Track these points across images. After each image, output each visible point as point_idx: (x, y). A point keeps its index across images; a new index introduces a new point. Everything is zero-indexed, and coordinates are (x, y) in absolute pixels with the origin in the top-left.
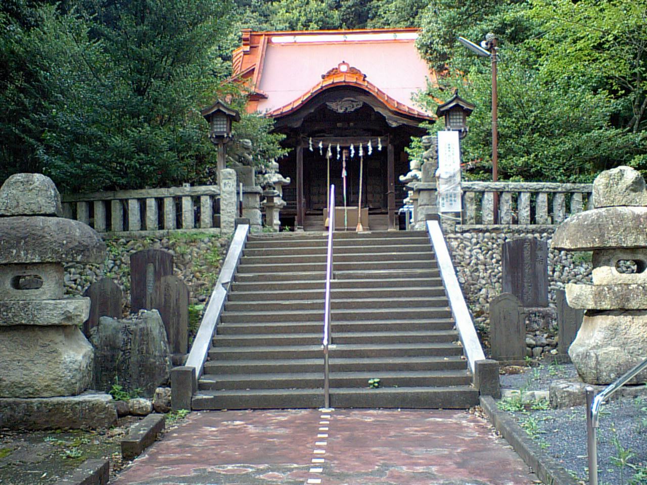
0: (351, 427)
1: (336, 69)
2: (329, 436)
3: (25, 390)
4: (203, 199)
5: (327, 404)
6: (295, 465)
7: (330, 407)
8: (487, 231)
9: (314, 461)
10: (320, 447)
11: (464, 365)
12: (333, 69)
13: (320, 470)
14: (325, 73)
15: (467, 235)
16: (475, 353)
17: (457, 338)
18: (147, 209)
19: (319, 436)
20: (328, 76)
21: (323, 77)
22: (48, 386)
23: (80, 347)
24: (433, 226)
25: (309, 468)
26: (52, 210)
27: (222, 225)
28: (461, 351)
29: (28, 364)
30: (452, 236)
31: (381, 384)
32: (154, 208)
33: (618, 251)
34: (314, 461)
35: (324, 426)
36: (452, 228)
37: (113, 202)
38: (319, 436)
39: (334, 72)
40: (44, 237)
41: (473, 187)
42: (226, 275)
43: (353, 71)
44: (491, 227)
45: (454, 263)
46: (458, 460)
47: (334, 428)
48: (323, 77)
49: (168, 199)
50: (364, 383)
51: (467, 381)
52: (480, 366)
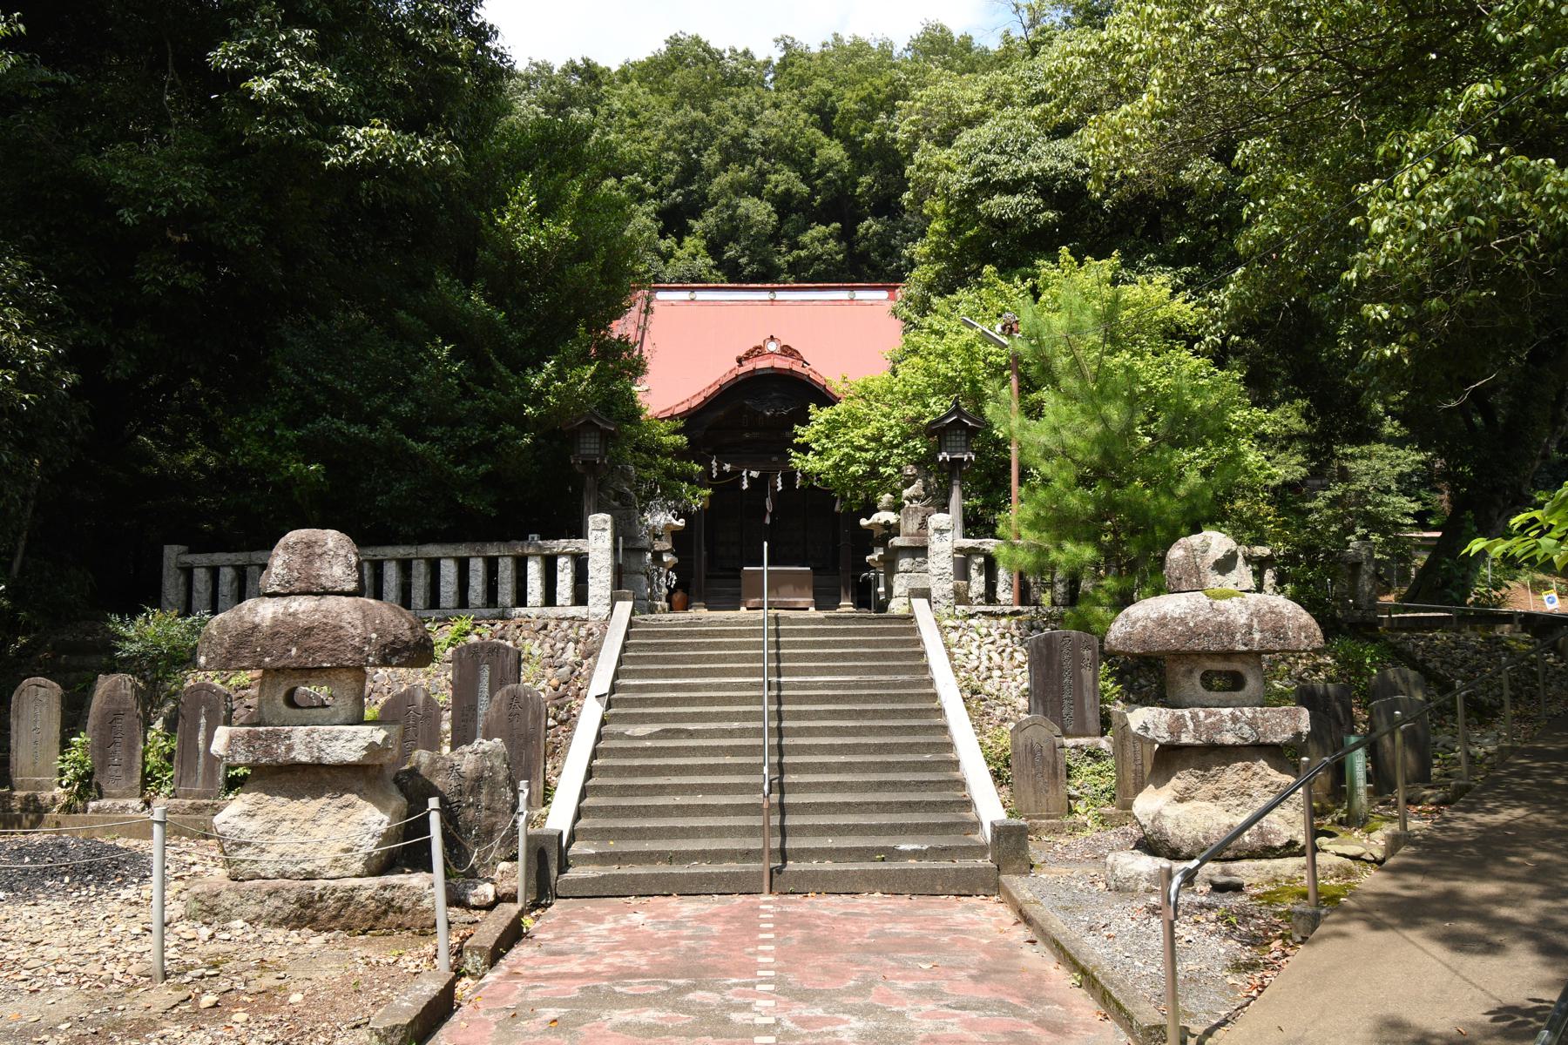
0: (803, 923)
1: (760, 348)
2: (778, 935)
3: (302, 865)
4: (561, 561)
5: (766, 888)
6: (734, 980)
7: (771, 892)
8: (1004, 615)
9: (760, 973)
10: (765, 954)
11: (976, 825)
12: (756, 348)
13: (771, 987)
14: (742, 354)
15: (973, 622)
16: (990, 807)
17: (961, 784)
18: (471, 574)
19: (762, 936)
20: (746, 359)
21: (740, 360)
22: (337, 860)
23: (389, 798)
24: (920, 605)
25: (753, 985)
26: (351, 586)
27: (590, 601)
28: (968, 804)
29: (307, 826)
30: (949, 623)
31: (602, 858)
32: (480, 573)
33: (1203, 659)
34: (760, 973)
35: (767, 921)
36: (950, 610)
37: (414, 562)
38: (762, 936)
39: (757, 352)
40: (341, 628)
41: (982, 547)
42: (601, 681)
43: (787, 351)
44: (1008, 610)
45: (953, 667)
46: (973, 972)
47: (782, 920)
48: (740, 360)
49: (506, 560)
50: (891, 854)
51: (981, 850)
52: (1000, 832)
